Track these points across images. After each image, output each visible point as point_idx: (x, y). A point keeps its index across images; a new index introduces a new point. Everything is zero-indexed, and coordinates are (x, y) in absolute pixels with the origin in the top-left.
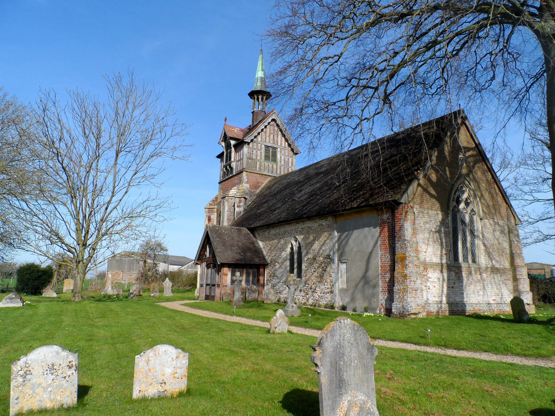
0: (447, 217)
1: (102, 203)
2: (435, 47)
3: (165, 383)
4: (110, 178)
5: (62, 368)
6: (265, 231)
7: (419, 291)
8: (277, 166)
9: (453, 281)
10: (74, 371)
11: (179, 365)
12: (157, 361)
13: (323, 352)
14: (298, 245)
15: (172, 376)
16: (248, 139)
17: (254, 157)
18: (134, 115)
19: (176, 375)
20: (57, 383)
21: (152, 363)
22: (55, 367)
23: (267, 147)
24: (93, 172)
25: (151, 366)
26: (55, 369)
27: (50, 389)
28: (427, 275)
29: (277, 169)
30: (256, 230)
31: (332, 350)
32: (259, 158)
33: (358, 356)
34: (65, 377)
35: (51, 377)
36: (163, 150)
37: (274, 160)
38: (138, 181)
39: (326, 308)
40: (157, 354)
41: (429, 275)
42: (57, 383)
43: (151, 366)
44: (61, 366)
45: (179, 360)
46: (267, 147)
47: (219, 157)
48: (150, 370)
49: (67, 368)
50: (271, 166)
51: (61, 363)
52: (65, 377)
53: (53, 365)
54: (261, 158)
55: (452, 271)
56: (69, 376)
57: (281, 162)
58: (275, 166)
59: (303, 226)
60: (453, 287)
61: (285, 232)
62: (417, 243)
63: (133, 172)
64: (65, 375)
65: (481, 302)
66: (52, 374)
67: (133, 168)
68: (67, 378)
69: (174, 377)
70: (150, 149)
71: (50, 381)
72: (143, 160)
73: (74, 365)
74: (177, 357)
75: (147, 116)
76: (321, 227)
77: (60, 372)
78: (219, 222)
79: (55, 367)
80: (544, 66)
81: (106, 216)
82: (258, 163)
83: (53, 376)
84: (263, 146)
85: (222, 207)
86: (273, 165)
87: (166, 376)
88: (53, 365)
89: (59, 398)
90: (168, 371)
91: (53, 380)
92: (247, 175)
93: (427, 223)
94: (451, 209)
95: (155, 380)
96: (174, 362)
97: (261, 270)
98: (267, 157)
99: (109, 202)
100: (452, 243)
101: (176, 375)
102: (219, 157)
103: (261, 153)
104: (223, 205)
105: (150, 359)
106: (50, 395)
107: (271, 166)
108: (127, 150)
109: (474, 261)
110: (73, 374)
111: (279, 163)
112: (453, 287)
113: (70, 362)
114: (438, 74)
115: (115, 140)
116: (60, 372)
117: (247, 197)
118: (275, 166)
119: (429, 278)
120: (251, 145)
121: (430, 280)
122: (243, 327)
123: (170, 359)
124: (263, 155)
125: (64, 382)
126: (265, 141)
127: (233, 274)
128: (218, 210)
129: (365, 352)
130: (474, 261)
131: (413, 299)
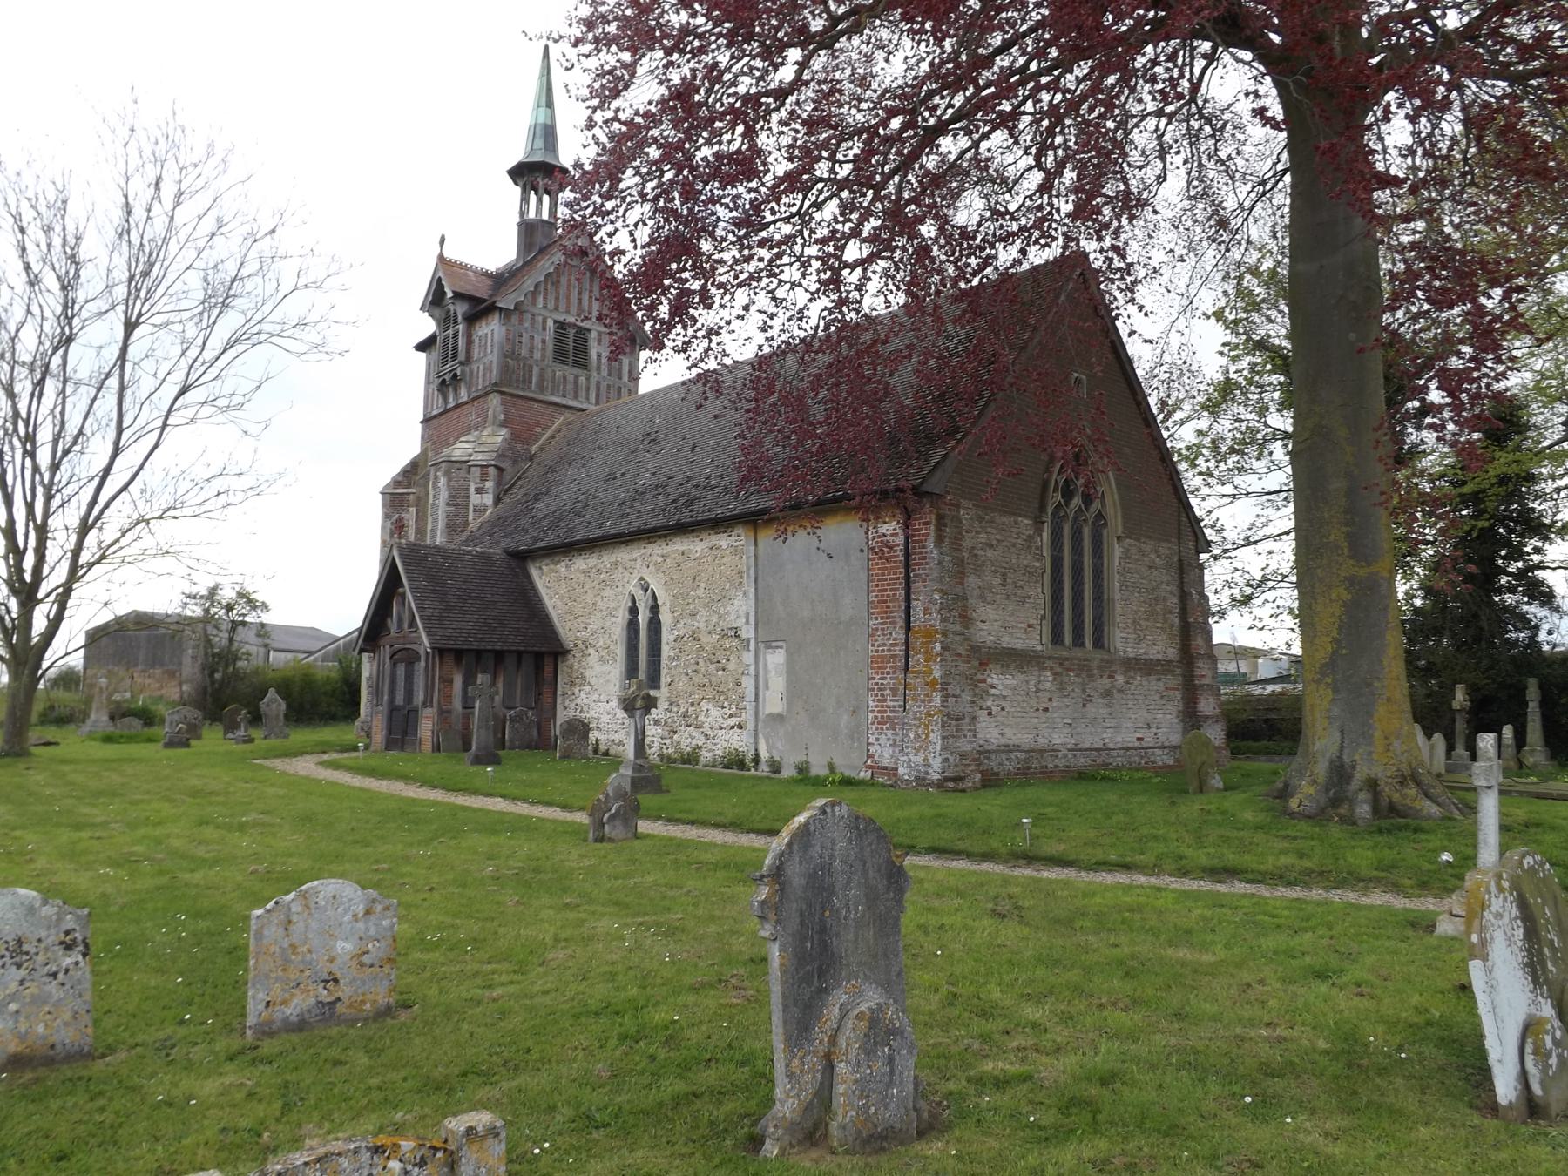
0: (1040, 531)
1: (84, 475)
2: (1010, 67)
3: (336, 981)
4: (108, 402)
5: (47, 949)
6: (558, 563)
7: (967, 720)
8: (588, 379)
9: (1048, 695)
10: (80, 958)
11: (372, 932)
12: (314, 925)
13: (782, 890)
14: (650, 602)
15: (354, 963)
16: (507, 302)
17: (524, 352)
18: (178, 221)
19: (366, 959)
20: (33, 989)
21: (298, 929)
22: (25, 948)
23: (561, 325)
24: (51, 387)
25: (295, 938)
26: (27, 953)
27: (13, 1007)
28: (984, 681)
29: (588, 389)
30: (534, 559)
31: (803, 882)
32: (537, 355)
33: (866, 895)
34: (54, 975)
35: (15, 974)
36: (266, 327)
37: (582, 362)
38: (189, 413)
39: (726, 767)
40: (312, 905)
41: (989, 681)
42: (33, 989)
43: (295, 938)
44: (42, 945)
45: (372, 918)
46: (561, 325)
47: (421, 347)
48: (293, 947)
49: (60, 951)
50: (571, 378)
51: (43, 934)
52: (54, 975)
53: (20, 942)
54: (543, 357)
55: (1045, 669)
56: (67, 971)
57: (599, 368)
58: (582, 379)
59: (666, 549)
60: (1046, 710)
61: (615, 565)
62: (964, 598)
63: (177, 389)
64: (54, 969)
65: (1111, 746)
66: (19, 966)
67: (178, 378)
68: (61, 976)
69: (362, 965)
70: (228, 324)
71: (13, 986)
72: (208, 355)
73: (80, 938)
74: (368, 912)
75: (221, 224)
76: (715, 552)
77: (40, 959)
78: (421, 531)
79: (25, 948)
80: (1285, 156)
81: (96, 511)
82: (536, 370)
83: (22, 973)
84: (550, 323)
85: (431, 493)
86: (576, 378)
87: (338, 962)
88: (20, 942)
89: (40, 1029)
90: (344, 947)
91: (22, 982)
92: (504, 403)
93: (991, 546)
94: (1050, 511)
95: (307, 973)
96: (361, 925)
97: (548, 670)
98: (560, 355)
99: (107, 471)
100: (1048, 598)
101: (366, 959)
102: (421, 347)
103: (544, 342)
104: (435, 487)
105: (294, 918)
106: (16, 1022)
107: (571, 378)
108: (158, 320)
109: (1098, 643)
110: (77, 963)
111: (595, 374)
112: (1046, 710)
113: (67, 933)
114: (1031, 161)
115: (120, 292)
116: (40, 959)
117: (503, 465)
118: (582, 379)
119: (992, 687)
120: (515, 319)
121: (993, 691)
122: (493, 825)
123: (348, 917)
124: (550, 346)
125: (52, 987)
126: (556, 308)
127: (469, 680)
128: (419, 498)
129: (881, 884)
130: (1098, 643)
131: (951, 741)
